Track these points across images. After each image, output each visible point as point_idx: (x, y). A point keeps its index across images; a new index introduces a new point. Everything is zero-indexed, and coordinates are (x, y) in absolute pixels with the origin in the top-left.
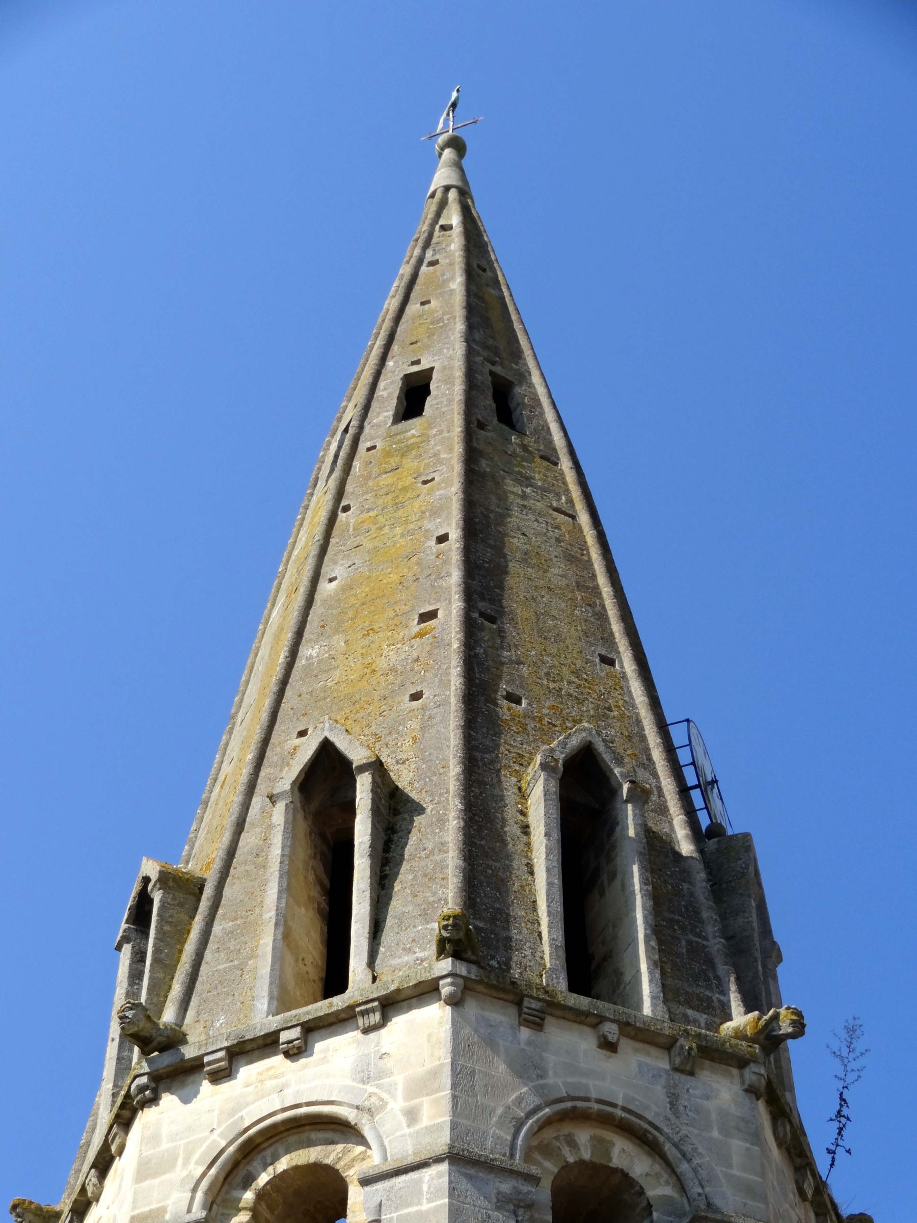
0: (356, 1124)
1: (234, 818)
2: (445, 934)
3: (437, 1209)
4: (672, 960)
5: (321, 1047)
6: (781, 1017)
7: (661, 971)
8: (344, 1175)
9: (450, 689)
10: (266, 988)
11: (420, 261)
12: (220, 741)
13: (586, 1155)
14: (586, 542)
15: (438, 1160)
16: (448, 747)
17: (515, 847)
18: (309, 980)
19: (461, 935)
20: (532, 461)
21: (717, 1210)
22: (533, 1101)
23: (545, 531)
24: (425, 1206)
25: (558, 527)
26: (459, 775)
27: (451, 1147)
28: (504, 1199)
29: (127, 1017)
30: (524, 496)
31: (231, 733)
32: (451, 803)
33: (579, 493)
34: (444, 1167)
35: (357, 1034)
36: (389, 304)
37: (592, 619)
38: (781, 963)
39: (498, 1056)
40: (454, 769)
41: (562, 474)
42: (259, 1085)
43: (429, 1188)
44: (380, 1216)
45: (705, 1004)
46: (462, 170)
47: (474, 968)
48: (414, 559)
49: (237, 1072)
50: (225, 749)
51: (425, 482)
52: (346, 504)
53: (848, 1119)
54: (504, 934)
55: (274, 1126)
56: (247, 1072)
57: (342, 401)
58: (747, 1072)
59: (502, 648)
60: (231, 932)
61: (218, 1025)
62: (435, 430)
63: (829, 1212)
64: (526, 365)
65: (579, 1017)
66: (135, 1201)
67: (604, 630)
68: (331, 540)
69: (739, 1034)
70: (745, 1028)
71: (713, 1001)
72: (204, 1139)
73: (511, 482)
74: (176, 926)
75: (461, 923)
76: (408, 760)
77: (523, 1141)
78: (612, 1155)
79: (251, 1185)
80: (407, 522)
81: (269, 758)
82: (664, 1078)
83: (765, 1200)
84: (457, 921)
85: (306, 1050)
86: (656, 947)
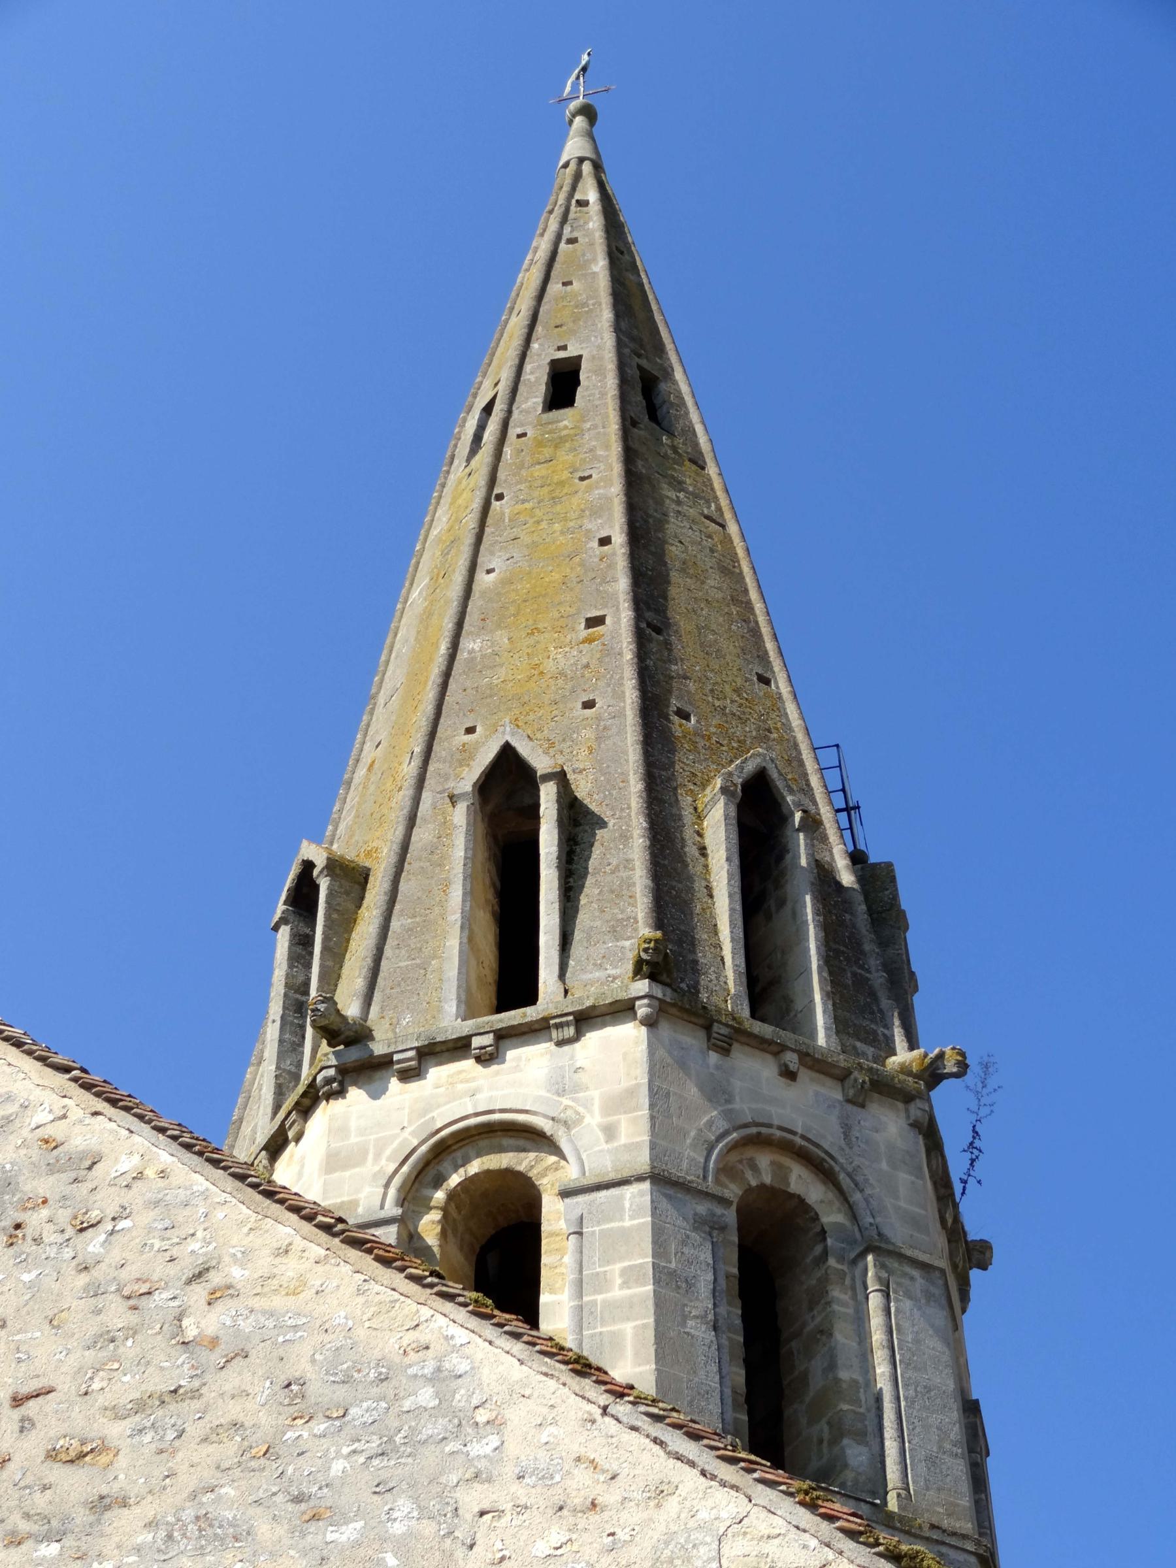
2: (644, 956)
3: (639, 1227)
5: (511, 1055)
8: (537, 1183)
9: (624, 701)
10: (454, 990)
13: (767, 1179)
14: (736, 554)
15: (640, 1179)
16: (627, 761)
17: (695, 869)
19: (660, 959)
20: (682, 465)
21: (887, 1241)
22: (722, 1125)
24: (627, 1223)
25: (710, 537)
29: (319, 1010)
30: (679, 502)
31: (372, 713)
34: (646, 1186)
36: (524, 277)
37: (747, 635)
39: (690, 1079)
40: (635, 786)
41: (710, 480)
43: (631, 1205)
47: (669, 991)
48: (577, 559)
49: (427, 1072)
50: (367, 730)
51: (582, 479)
52: (499, 492)
53: (980, 1151)
54: (691, 957)
55: (467, 1130)
56: (438, 1074)
57: (476, 376)
58: (912, 1107)
59: (670, 661)
60: (411, 930)
61: (405, 1023)
62: (590, 424)
67: (759, 648)
69: (905, 1070)
70: (910, 1064)
72: (395, 1136)
73: (666, 486)
74: (343, 914)
76: (585, 770)
80: (565, 519)
81: (436, 752)
85: (497, 1057)
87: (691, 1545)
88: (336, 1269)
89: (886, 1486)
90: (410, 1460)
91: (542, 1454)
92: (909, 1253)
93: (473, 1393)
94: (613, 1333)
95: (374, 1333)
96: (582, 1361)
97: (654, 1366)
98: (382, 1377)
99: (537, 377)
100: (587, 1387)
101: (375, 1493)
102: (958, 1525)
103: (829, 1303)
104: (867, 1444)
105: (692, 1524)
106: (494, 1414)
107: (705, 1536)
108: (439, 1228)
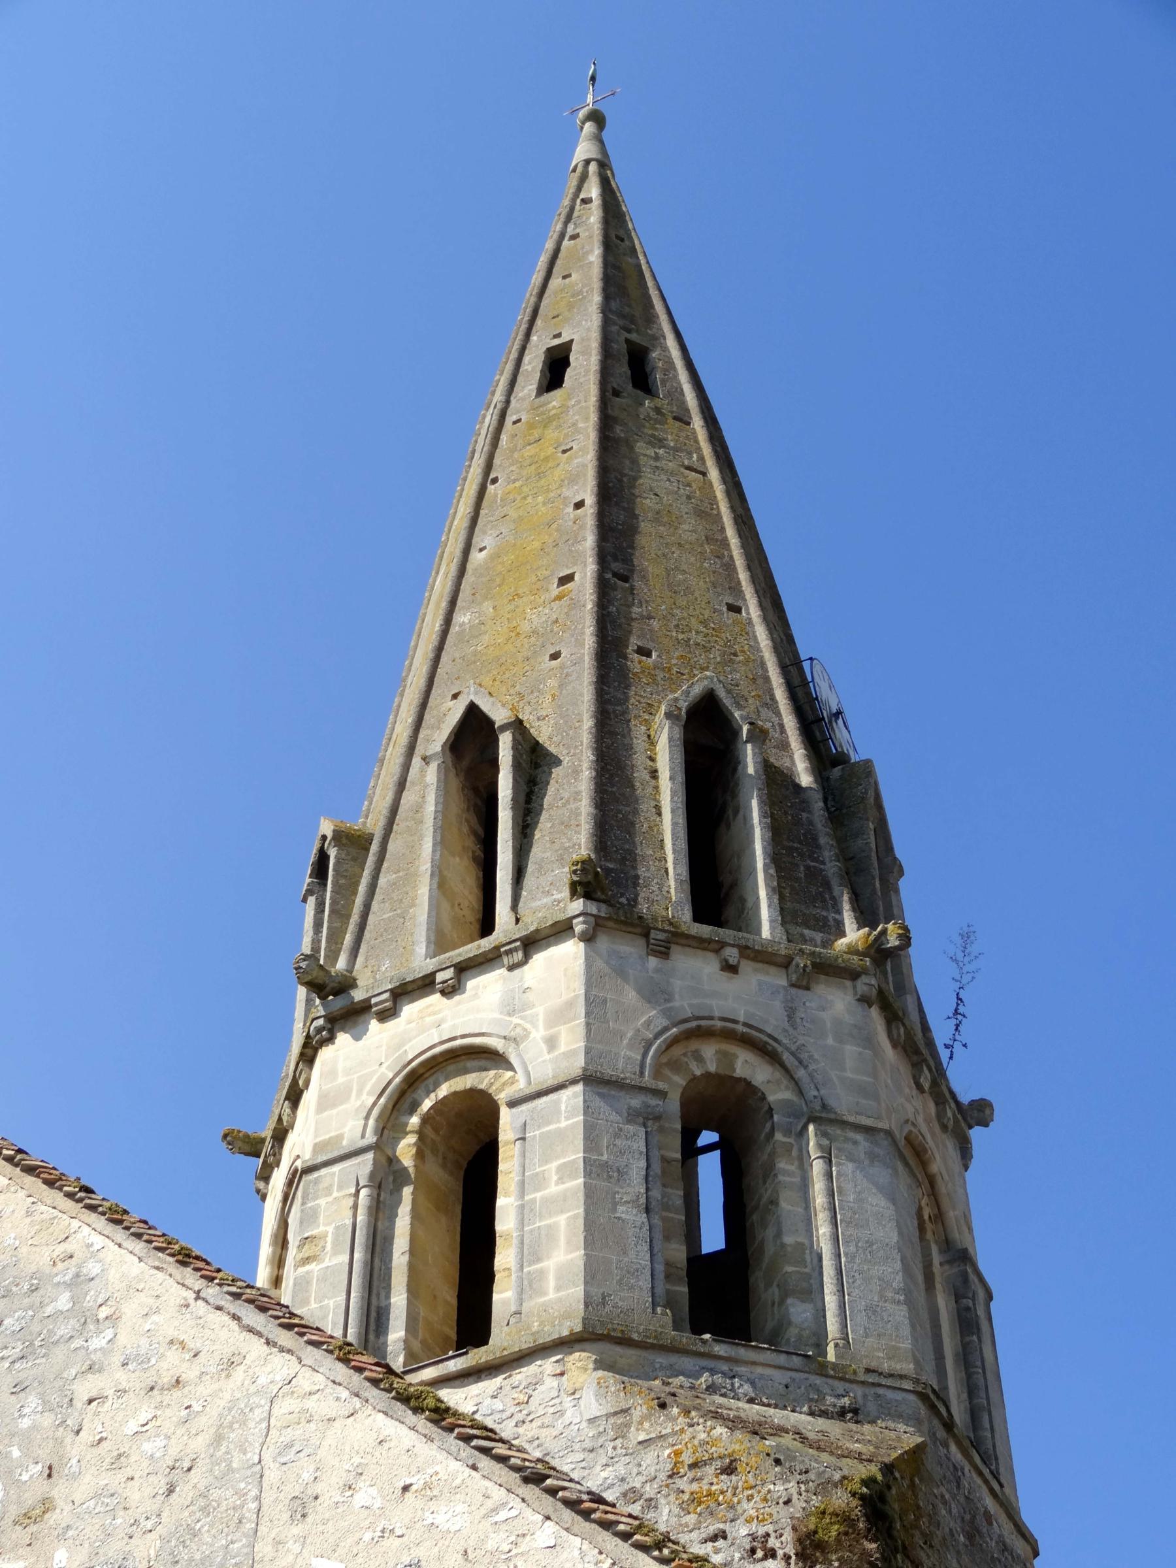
1: (395, 778)
2: (576, 878)
3: (573, 1126)
5: (471, 984)
8: (496, 1098)
10: (424, 933)
11: (562, 236)
12: (393, 702)
13: (712, 1068)
15: (574, 1082)
19: (590, 877)
23: (676, 489)
24: (563, 1124)
25: (689, 485)
26: (591, 728)
27: (585, 1069)
30: (657, 458)
31: (402, 695)
32: (584, 754)
33: (710, 450)
34: (579, 1088)
35: (502, 971)
37: (721, 570)
40: (588, 723)
41: (694, 432)
43: (566, 1107)
46: (601, 142)
47: (604, 907)
48: (554, 526)
49: (401, 1010)
50: (398, 711)
51: (564, 452)
53: (964, 1016)
54: (632, 873)
55: (434, 1057)
56: (410, 1010)
57: (495, 375)
60: (394, 884)
63: (947, 1101)
64: (662, 330)
65: (702, 944)
66: (316, 1130)
68: (482, 512)
69: (852, 950)
72: (375, 1072)
75: (588, 867)
80: (548, 491)
85: (459, 988)
88: (15, 1195)
90: (44, 1360)
91: (144, 1342)
92: (851, 1119)
93: (100, 1293)
94: (549, 1226)
95: (34, 1249)
96: (183, 1252)
97: (583, 1252)
98: (33, 1288)
99: (534, 364)
100: (188, 1275)
101: (12, 1393)
102: (898, 1367)
103: (776, 1175)
104: (812, 1301)
105: (253, 1389)
106: (113, 1310)
108: (415, 1149)
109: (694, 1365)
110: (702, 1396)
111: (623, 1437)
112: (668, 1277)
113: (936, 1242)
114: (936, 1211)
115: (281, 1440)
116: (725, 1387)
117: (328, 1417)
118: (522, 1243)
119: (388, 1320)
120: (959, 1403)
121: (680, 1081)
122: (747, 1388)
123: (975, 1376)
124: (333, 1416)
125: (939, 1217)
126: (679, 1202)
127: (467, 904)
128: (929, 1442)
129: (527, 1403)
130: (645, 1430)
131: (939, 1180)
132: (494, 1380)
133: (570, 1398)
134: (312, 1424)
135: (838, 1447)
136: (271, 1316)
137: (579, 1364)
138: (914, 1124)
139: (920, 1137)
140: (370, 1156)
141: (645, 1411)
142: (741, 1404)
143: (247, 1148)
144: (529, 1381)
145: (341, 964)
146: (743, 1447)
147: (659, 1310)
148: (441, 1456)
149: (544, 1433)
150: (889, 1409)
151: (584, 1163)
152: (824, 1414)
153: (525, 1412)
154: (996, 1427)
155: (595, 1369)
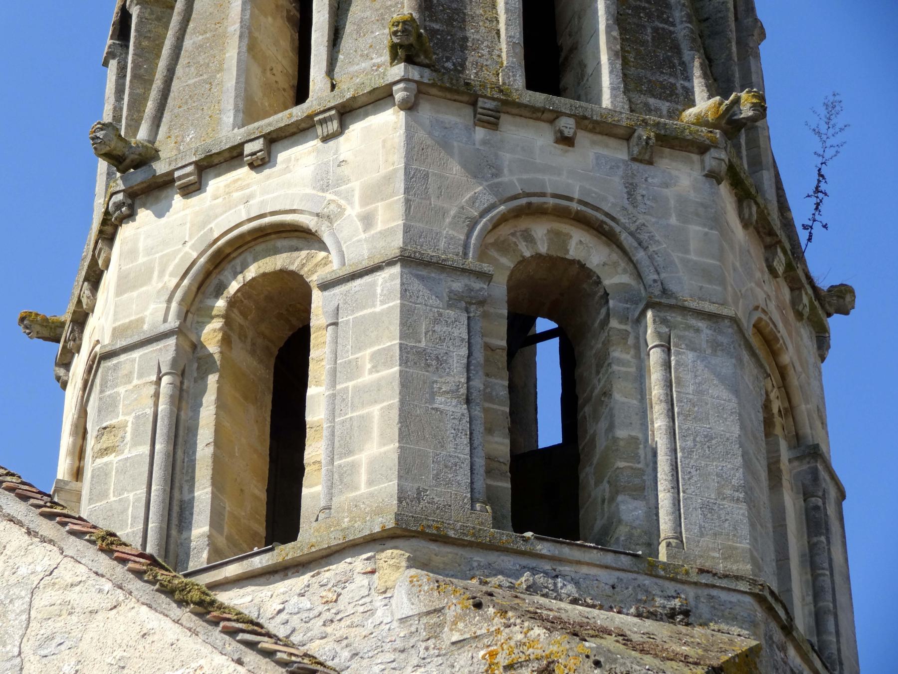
0: (316, 231)
2: (396, 40)
4: (636, 49)
5: (283, 156)
6: (742, 101)
7: (622, 60)
8: (308, 280)
10: (232, 101)
13: (543, 249)
15: (390, 263)
18: (279, 89)
19: (412, 40)
22: (488, 199)
24: (378, 309)
27: (403, 250)
28: (456, 297)
29: (99, 138)
34: (396, 270)
35: (315, 143)
38: (765, 41)
42: (226, 197)
43: (382, 290)
44: (338, 319)
45: (668, 92)
47: (427, 72)
49: (207, 185)
53: (826, 194)
54: (460, 35)
55: (241, 236)
56: (216, 185)
58: (707, 157)
60: (201, 46)
61: (188, 139)
65: (535, 113)
66: (116, 313)
69: (701, 121)
71: (676, 89)
72: (179, 250)
74: (154, 41)
75: (410, 28)
77: (476, 239)
78: (568, 248)
79: (222, 294)
82: (621, 169)
83: (722, 282)
84: (406, 27)
85: (269, 161)
86: (618, 37)
87: (9, 600)
89: (659, 537)
92: (693, 305)
97: (397, 445)
102: (735, 568)
103: (609, 365)
104: (644, 498)
105: (13, 580)
107: (21, 591)
108: (221, 335)
109: (514, 564)
110: (522, 596)
111: (436, 637)
112: (489, 472)
113: (785, 437)
114: (787, 405)
115: (42, 632)
116: (546, 587)
117: (90, 609)
118: (333, 434)
119: (192, 514)
120: (803, 605)
121: (507, 262)
122: (571, 588)
123: (822, 578)
124: (95, 608)
125: (790, 411)
126: (504, 393)
127: (280, 68)
128: (764, 646)
129: (336, 601)
130: (459, 631)
131: (791, 372)
132: (302, 577)
133: (380, 597)
134: (73, 617)
135: (663, 650)
136: (32, 505)
137: (391, 562)
138: (764, 311)
139: (771, 325)
140: (172, 341)
141: (459, 611)
142: (563, 605)
143: (46, 333)
144: (338, 579)
145: (142, 134)
146: (561, 648)
147: (478, 506)
148: (206, 650)
149: (353, 632)
150: (723, 611)
151: (401, 350)
152: (652, 616)
153: (333, 611)
154: (842, 631)
155: (408, 567)
